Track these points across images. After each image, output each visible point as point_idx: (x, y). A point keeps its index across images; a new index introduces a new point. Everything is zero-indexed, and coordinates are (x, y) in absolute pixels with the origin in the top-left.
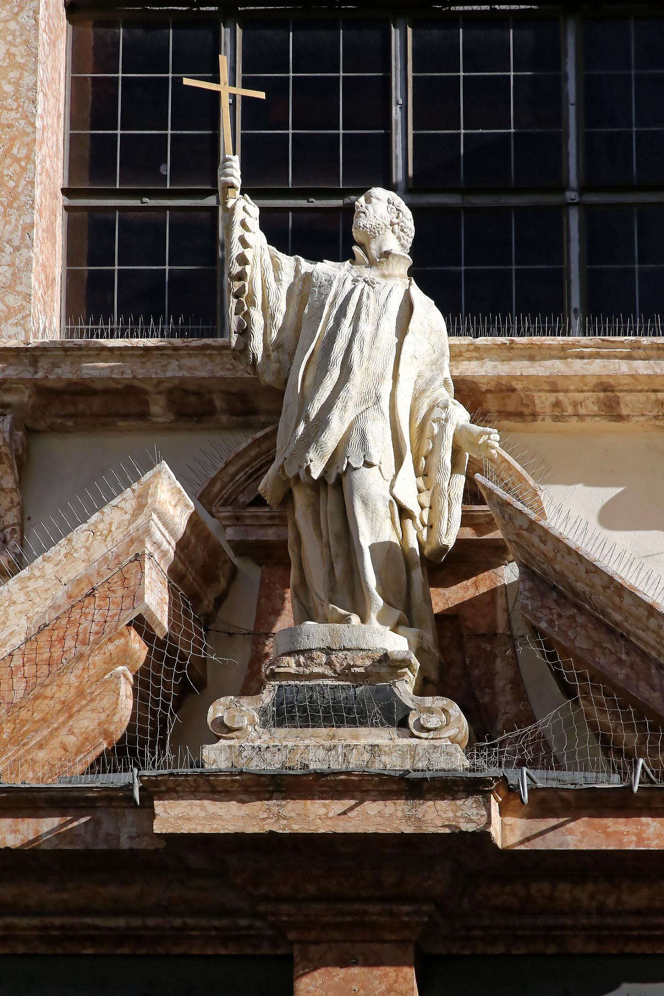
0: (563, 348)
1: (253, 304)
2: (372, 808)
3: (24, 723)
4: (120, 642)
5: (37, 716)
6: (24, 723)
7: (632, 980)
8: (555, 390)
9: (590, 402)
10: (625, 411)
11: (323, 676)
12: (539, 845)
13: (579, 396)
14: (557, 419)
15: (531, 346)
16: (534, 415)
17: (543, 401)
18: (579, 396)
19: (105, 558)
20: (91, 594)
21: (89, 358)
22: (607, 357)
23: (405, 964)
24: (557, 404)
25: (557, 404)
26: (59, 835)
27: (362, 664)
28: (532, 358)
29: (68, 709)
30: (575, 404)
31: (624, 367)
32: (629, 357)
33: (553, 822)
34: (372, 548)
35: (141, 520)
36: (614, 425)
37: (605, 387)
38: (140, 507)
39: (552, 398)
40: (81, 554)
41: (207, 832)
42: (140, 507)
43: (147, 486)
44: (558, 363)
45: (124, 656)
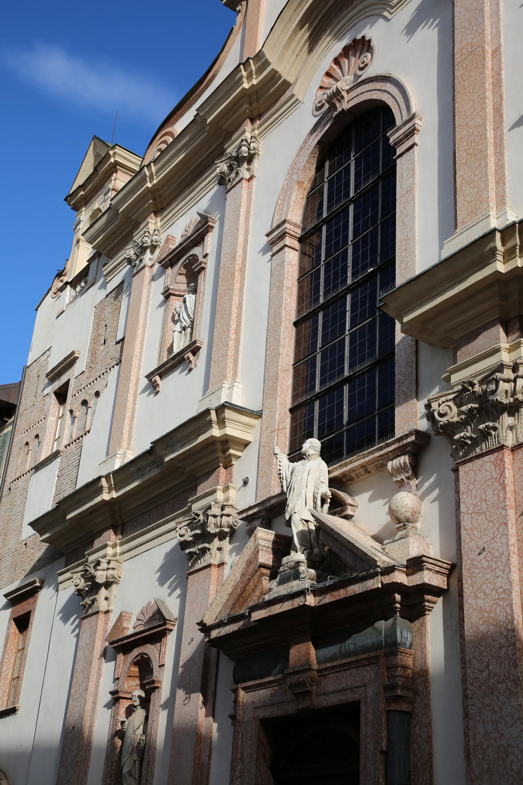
0: (351, 461)
1: (283, 479)
2: (286, 604)
3: (244, 597)
4: (259, 572)
5: (247, 595)
6: (244, 597)
7: (354, 634)
8: (354, 471)
9: (362, 471)
10: (370, 470)
11: (287, 570)
12: (321, 603)
13: (359, 471)
14: (358, 478)
15: (345, 463)
16: (353, 478)
17: (353, 475)
18: (359, 471)
19: (251, 554)
20: (251, 563)
21: (271, 500)
22: (360, 459)
23: (307, 641)
24: (356, 474)
25: (356, 474)
26: (243, 625)
27: (292, 564)
28: (346, 466)
29: (254, 590)
30: (360, 473)
31: (363, 461)
32: (364, 458)
33: (324, 596)
34: (297, 534)
35: (256, 542)
36: (370, 474)
37: (363, 466)
38: (255, 539)
39: (354, 473)
40: (246, 555)
41: (434, 584)
42: (255, 539)
43: (256, 534)
44: (351, 465)
45: (263, 575)
